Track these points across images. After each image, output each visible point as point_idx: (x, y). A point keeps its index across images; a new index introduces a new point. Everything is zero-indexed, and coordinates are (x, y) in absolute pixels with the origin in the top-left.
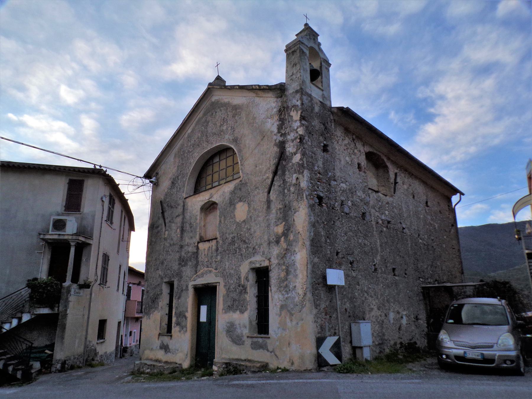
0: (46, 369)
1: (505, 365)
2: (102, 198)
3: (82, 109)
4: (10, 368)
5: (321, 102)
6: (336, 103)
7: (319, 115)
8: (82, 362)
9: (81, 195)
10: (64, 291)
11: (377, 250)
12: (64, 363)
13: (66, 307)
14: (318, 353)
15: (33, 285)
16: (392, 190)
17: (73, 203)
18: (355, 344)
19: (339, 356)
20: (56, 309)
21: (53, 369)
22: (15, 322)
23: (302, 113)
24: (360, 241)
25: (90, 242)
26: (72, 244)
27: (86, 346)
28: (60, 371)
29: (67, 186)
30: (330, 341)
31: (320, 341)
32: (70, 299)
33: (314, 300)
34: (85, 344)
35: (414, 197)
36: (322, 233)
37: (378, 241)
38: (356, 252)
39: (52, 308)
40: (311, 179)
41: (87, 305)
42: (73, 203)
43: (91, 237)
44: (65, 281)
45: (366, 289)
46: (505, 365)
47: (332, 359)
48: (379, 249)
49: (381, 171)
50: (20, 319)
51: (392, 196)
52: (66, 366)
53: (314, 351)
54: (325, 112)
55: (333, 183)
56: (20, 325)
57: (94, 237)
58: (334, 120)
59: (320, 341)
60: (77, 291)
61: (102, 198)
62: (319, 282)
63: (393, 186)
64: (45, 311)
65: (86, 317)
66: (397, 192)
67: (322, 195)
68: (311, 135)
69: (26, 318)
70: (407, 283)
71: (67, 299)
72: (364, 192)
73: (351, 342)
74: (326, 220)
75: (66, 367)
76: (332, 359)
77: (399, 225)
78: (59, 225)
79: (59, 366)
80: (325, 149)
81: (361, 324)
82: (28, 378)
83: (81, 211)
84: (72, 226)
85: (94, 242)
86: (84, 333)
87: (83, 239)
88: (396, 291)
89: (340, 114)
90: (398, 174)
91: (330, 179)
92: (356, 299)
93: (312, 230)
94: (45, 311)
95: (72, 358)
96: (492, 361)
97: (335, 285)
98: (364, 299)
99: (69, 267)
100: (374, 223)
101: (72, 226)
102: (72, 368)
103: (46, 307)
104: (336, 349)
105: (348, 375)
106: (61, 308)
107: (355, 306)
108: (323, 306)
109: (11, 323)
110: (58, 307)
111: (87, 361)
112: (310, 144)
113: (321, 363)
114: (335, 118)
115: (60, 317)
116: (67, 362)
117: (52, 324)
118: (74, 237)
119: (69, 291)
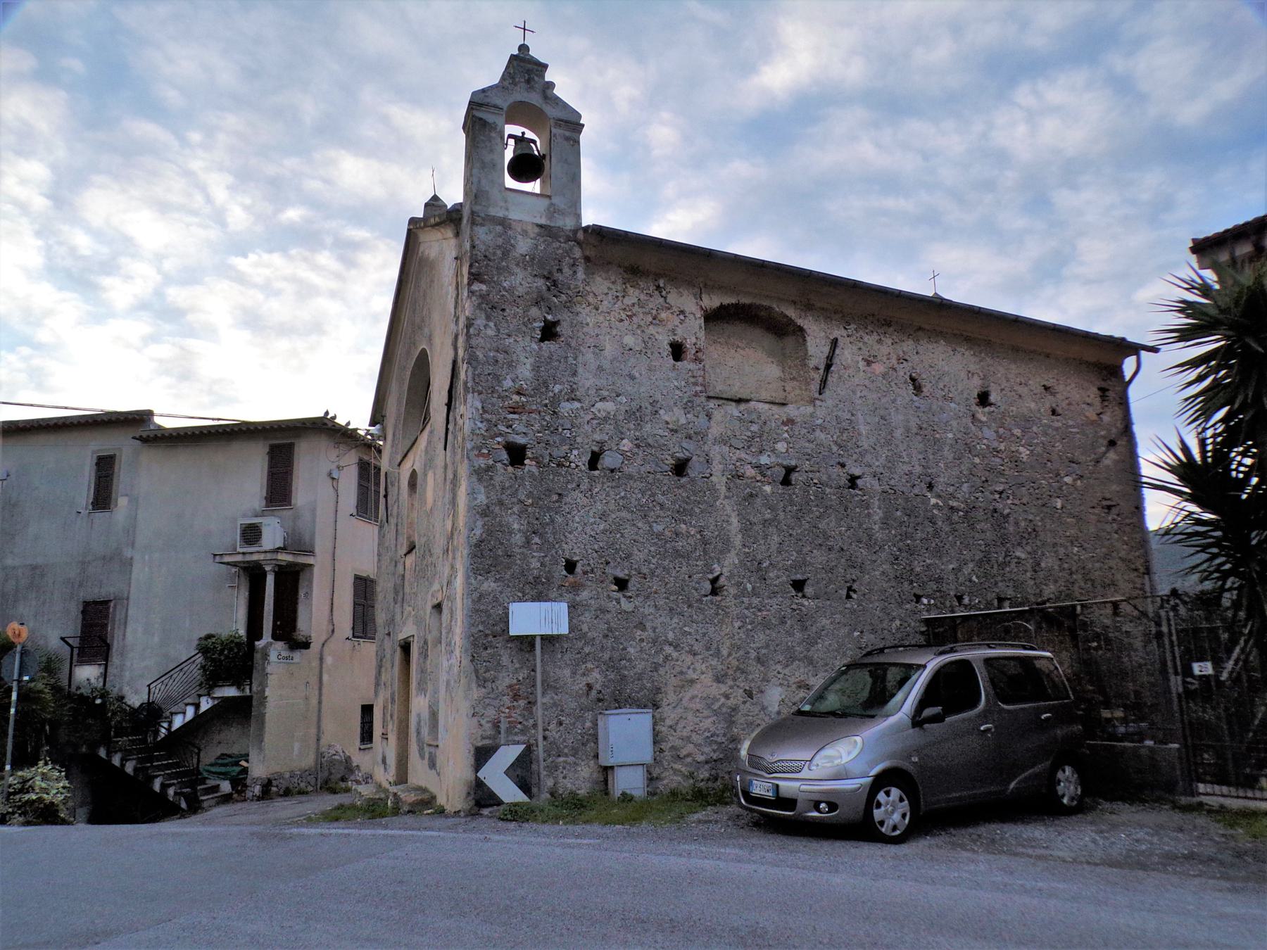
0: (239, 792)
1: (816, 814)
2: (330, 474)
3: (251, 307)
4: (171, 791)
5: (541, 226)
6: (589, 217)
7: (533, 259)
8: (313, 782)
9: (292, 471)
10: (257, 656)
11: (727, 543)
12: (267, 786)
13: (263, 686)
14: (477, 779)
15: (207, 647)
16: (815, 386)
17: (279, 491)
18: (605, 760)
19: (525, 787)
20: (248, 691)
21: (249, 794)
22: (190, 712)
23: (471, 266)
24: (658, 528)
25: (310, 560)
26: (268, 568)
27: (320, 755)
28: (259, 799)
29: (267, 458)
30: (508, 754)
31: (482, 755)
32: (269, 669)
33: (476, 671)
34: (318, 749)
35: (918, 388)
36: (516, 526)
37: (734, 520)
38: (639, 556)
39: (239, 686)
40: (485, 411)
41: (314, 680)
42: (279, 491)
43: (311, 552)
44: (260, 637)
45: (671, 636)
46: (816, 814)
47: (509, 793)
48: (737, 540)
49: (790, 342)
50: (197, 706)
51: (812, 401)
52: (274, 789)
53: (468, 774)
54: (556, 245)
55: (566, 407)
56: (197, 717)
57: (317, 550)
58: (587, 259)
59: (482, 755)
60: (285, 654)
61: (330, 474)
62: (490, 634)
63: (817, 377)
64: (231, 692)
65: (314, 701)
66: (827, 393)
67: (521, 440)
68: (497, 314)
69: (205, 705)
70: (853, 612)
71: (264, 669)
72: (688, 407)
73: (596, 756)
74: (530, 495)
75: (267, 791)
76: (509, 793)
77: (838, 469)
78: (251, 534)
79: (257, 790)
80: (549, 332)
81: (611, 718)
82: (195, 807)
83: (293, 502)
84: (272, 535)
85: (319, 562)
86: (313, 731)
87: (289, 558)
88: (798, 635)
89: (592, 240)
90: (840, 343)
91: (555, 401)
92: (630, 660)
93: (479, 523)
94: (231, 692)
95: (287, 775)
96: (789, 803)
97: (533, 637)
98: (661, 659)
99: (266, 608)
100: (719, 480)
101: (272, 535)
102: (287, 793)
103: (232, 685)
104: (522, 773)
105: (513, 825)
106: (254, 689)
107: (623, 677)
108: (505, 681)
109: (184, 713)
110: (251, 685)
111: (326, 782)
112: (490, 332)
113: (482, 798)
114: (588, 253)
115: (254, 703)
116: (274, 783)
117: (241, 712)
118: (269, 556)
119: (265, 656)
